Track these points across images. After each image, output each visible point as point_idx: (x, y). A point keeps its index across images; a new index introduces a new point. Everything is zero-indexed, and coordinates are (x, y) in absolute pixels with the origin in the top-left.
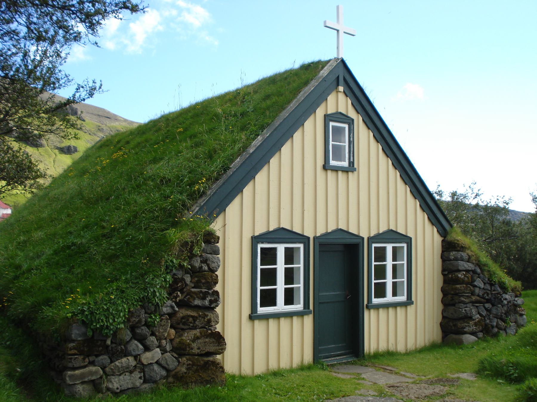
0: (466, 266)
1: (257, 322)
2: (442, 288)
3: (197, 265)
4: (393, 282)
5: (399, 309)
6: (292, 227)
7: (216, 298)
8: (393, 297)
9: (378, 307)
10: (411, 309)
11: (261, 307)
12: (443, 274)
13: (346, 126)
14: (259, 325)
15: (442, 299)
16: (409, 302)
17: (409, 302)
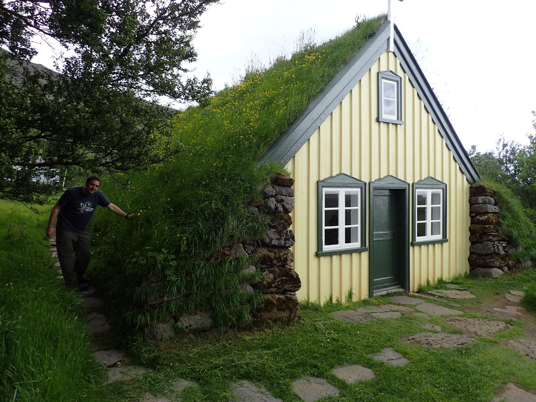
0: (493, 209)
1: (322, 259)
2: (469, 228)
3: (273, 207)
4: (346, 229)
5: (436, 245)
6: (351, 172)
7: (291, 237)
8: (346, 243)
9: (420, 244)
10: (446, 245)
11: (325, 245)
12: (470, 216)
13: (395, 83)
14: (324, 260)
15: (470, 237)
16: (445, 239)
17: (445, 239)
